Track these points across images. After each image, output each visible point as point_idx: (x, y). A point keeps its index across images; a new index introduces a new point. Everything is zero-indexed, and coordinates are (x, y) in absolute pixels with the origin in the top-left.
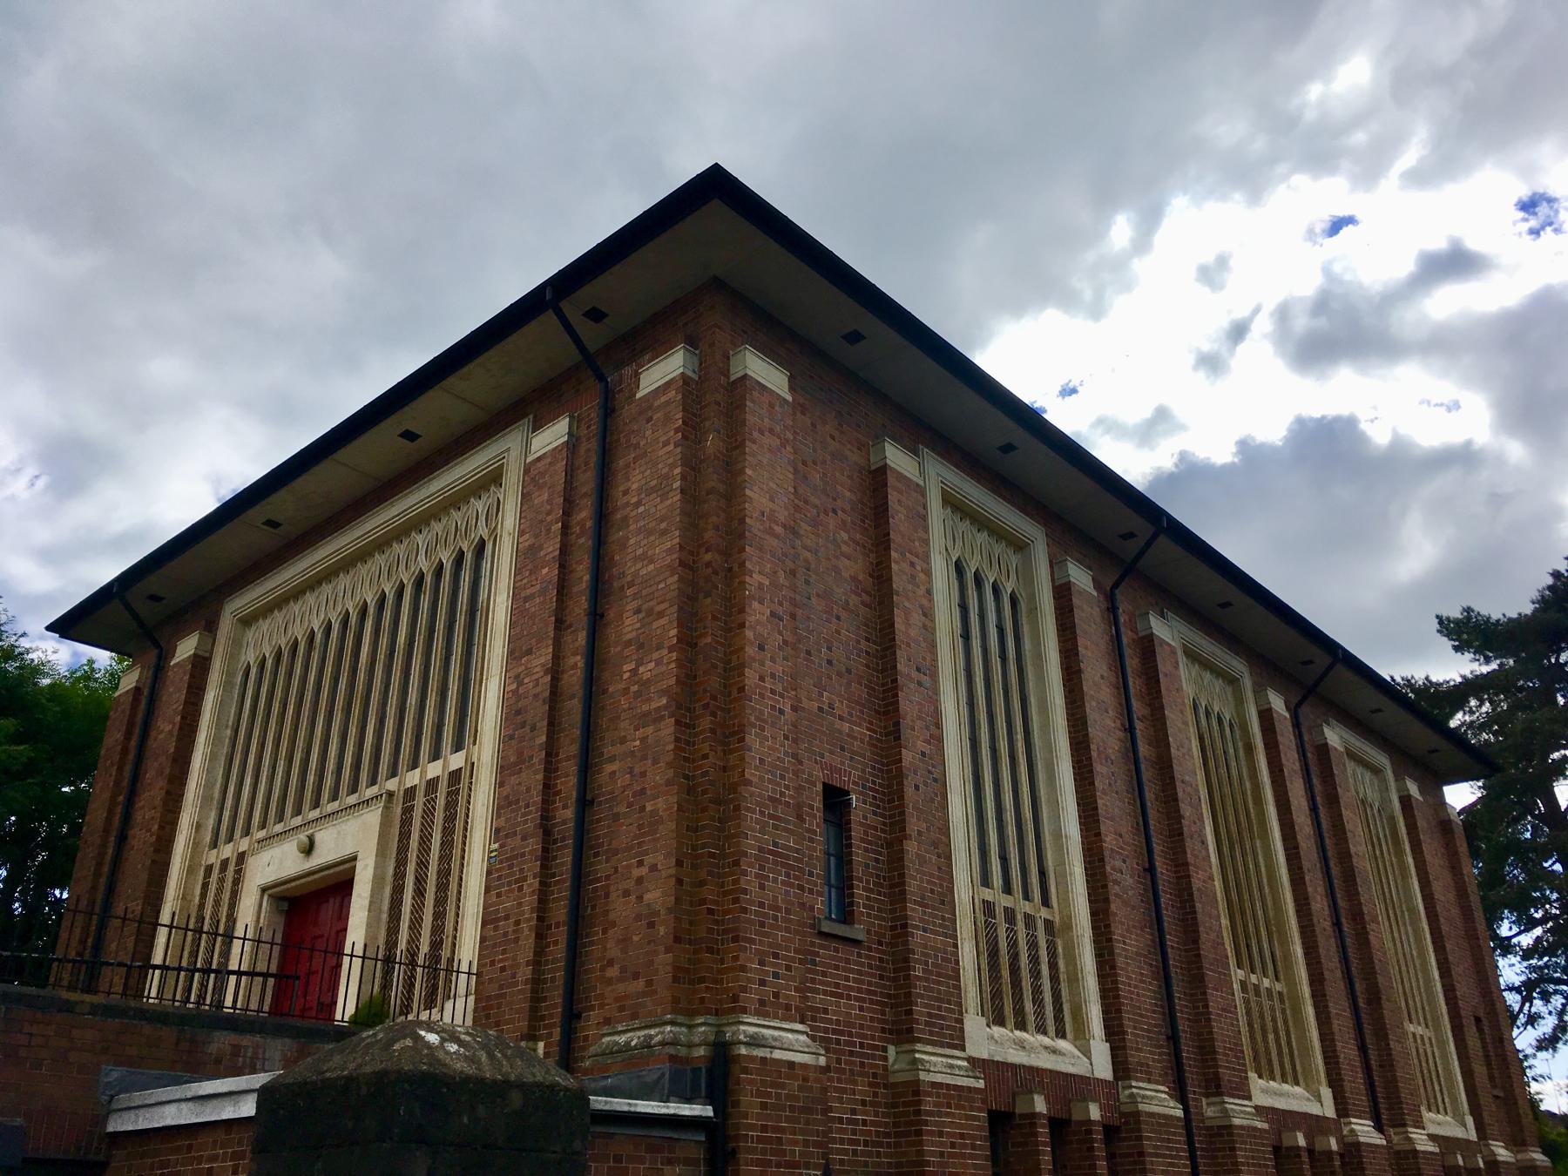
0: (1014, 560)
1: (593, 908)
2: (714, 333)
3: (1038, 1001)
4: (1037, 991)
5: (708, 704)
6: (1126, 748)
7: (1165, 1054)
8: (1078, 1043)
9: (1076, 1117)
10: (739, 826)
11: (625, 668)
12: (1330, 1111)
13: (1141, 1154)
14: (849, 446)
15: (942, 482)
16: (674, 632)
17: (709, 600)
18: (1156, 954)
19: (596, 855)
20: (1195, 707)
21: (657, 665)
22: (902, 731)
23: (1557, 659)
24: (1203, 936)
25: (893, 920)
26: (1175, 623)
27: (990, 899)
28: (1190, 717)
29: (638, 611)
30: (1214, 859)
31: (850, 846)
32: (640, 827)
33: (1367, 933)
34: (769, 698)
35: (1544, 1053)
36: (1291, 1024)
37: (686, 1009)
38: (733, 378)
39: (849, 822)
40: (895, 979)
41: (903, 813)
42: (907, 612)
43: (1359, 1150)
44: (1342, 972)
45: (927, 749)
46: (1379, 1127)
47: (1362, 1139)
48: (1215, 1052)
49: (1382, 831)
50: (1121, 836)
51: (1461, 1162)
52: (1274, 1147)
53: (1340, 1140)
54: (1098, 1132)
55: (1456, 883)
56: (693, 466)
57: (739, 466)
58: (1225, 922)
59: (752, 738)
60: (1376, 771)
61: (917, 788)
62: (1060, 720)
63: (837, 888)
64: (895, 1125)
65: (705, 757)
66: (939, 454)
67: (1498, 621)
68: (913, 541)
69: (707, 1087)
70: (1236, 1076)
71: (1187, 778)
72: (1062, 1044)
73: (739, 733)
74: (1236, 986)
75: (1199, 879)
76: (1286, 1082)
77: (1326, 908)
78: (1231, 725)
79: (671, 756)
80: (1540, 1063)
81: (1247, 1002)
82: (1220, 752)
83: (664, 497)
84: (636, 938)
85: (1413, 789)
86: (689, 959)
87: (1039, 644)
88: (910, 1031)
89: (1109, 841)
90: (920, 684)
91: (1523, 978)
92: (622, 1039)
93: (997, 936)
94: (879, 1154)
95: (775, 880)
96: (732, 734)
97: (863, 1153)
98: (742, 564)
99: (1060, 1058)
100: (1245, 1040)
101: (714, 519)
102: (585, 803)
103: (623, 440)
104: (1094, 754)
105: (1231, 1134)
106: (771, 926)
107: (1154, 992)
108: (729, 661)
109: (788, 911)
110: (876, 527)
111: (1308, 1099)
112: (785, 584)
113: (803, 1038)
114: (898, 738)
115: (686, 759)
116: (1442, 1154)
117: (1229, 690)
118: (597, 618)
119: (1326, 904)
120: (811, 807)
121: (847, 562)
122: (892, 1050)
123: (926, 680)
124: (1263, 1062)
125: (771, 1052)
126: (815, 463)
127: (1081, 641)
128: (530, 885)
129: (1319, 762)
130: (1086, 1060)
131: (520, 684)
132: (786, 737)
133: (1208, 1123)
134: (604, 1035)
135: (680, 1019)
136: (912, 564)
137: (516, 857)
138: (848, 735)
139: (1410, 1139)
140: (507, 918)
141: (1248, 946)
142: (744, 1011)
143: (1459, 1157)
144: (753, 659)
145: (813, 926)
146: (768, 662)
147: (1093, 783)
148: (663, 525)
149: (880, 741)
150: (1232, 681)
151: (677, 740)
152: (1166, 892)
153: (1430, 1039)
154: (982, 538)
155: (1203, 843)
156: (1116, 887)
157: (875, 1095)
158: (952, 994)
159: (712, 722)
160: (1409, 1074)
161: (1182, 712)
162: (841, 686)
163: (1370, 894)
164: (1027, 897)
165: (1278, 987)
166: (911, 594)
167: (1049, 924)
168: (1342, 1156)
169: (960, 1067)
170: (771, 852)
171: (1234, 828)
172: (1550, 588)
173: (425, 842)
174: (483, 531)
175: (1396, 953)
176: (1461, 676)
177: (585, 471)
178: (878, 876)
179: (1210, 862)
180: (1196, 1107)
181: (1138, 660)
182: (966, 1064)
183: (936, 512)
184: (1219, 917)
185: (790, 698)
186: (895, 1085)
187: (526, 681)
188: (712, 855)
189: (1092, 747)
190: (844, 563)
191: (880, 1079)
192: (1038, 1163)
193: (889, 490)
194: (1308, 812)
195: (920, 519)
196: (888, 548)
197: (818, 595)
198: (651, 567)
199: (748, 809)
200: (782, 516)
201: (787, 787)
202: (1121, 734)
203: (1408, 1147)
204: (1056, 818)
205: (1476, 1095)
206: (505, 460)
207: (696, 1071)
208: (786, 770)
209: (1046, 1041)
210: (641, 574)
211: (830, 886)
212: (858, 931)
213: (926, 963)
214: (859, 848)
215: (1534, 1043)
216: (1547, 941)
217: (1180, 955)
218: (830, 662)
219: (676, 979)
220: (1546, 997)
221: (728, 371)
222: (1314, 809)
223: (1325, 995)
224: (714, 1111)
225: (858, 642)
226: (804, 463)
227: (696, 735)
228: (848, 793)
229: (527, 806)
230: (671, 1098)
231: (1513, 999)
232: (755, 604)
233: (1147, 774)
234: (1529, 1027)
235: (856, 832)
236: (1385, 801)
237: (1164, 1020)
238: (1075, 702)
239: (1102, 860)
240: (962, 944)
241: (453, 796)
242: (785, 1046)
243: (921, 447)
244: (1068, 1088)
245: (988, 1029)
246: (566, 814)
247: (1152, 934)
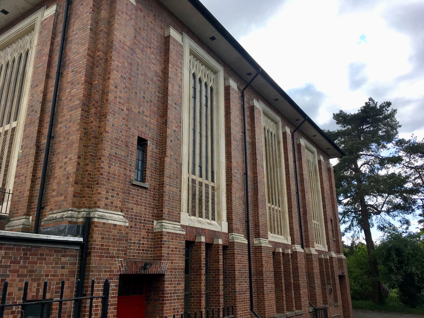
0: (213, 76)
1: (51, 172)
4: (207, 206)
6: (242, 138)
8: (219, 222)
9: (215, 243)
10: (102, 146)
11: (67, 91)
12: (290, 243)
13: (234, 254)
14: (157, 27)
16: (84, 78)
17: (97, 69)
18: (245, 198)
19: (53, 155)
20: (265, 129)
22: (168, 123)
24: (259, 193)
25: (159, 182)
26: (261, 103)
27: (195, 178)
29: (73, 71)
30: (265, 172)
31: (146, 158)
32: (67, 145)
33: (305, 196)
34: (118, 105)
36: (282, 219)
37: (77, 206)
39: (147, 150)
41: (166, 149)
42: (173, 85)
43: (296, 253)
46: (303, 247)
47: (297, 250)
48: (259, 226)
49: (312, 168)
50: (238, 163)
51: (323, 257)
52: (273, 252)
53: (292, 250)
54: (221, 247)
55: (330, 184)
56: (96, 22)
57: (113, 23)
58: (266, 190)
59: (110, 117)
60: (313, 153)
61: (171, 141)
62: (222, 127)
63: (141, 171)
65: (92, 122)
66: (190, 37)
67: (349, 115)
68: (177, 62)
69: (82, 231)
70: (264, 232)
71: (260, 148)
72: (213, 222)
74: (267, 208)
75: (260, 177)
77: (295, 188)
78: (274, 136)
79: (79, 121)
81: (270, 212)
82: (270, 143)
83: (85, 31)
84: (63, 182)
85: (322, 158)
88: (162, 216)
89: (234, 164)
90: (175, 108)
92: (54, 216)
96: (103, 115)
97: (142, 253)
98: (111, 57)
99: (212, 226)
101: (102, 40)
102: (51, 137)
103: (74, 13)
104: (232, 138)
105: (261, 248)
106: (112, 180)
107: (243, 208)
108: (104, 91)
109: (119, 176)
110: (165, 56)
111: (284, 239)
112: (128, 67)
113: (122, 217)
114: (166, 125)
116: (318, 255)
117: (275, 125)
118: (60, 74)
121: (154, 66)
122: (155, 222)
123: (178, 108)
124: (273, 228)
125: (107, 221)
126: (144, 30)
127: (231, 104)
128: (30, 165)
129: (297, 149)
130: (220, 226)
131: (33, 97)
132: (123, 119)
134: (49, 214)
135: (75, 209)
136: (176, 70)
137: (27, 155)
139: (310, 251)
140: (23, 175)
142: (99, 207)
143: (323, 256)
145: (130, 182)
146: (118, 93)
147: (231, 147)
148: (83, 41)
150: (276, 123)
151: (82, 115)
154: (203, 67)
155: (262, 167)
157: (148, 235)
158: (177, 206)
159: (95, 110)
162: (148, 106)
163: (307, 185)
164: (201, 176)
165: (279, 209)
166: (175, 79)
167: (213, 188)
168: (292, 255)
169: (177, 228)
170: (114, 156)
171: (272, 165)
173: (3, 151)
174: (28, 47)
175: (312, 202)
176: (337, 130)
177: (60, 24)
178: (155, 168)
182: (180, 227)
183: (187, 57)
184: (264, 188)
185: (126, 106)
186: (155, 233)
187: (35, 96)
188: (91, 155)
189: (232, 136)
190: (152, 65)
191: (150, 231)
192: (201, 256)
193: (170, 44)
195: (181, 56)
196: (168, 63)
197: (141, 74)
198: (78, 56)
200: (128, 43)
202: (241, 134)
203: (310, 253)
206: (36, 22)
208: (123, 130)
209: (208, 221)
211: (138, 170)
212: (146, 185)
213: (169, 196)
214: (150, 158)
216: (351, 202)
218: (144, 97)
219: (74, 196)
222: (295, 161)
223: (292, 212)
224: (83, 240)
225: (155, 92)
226: (140, 29)
227: (89, 115)
229: (32, 138)
230: (68, 235)
231: (340, 217)
232: (115, 72)
233: (248, 146)
234: (343, 224)
235: (149, 153)
236: (314, 161)
238: (228, 122)
239: (231, 169)
240: (183, 191)
241: (12, 135)
242: (114, 219)
243: (184, 33)
244: (214, 234)
245: (189, 217)
246: (44, 141)
247: (245, 192)
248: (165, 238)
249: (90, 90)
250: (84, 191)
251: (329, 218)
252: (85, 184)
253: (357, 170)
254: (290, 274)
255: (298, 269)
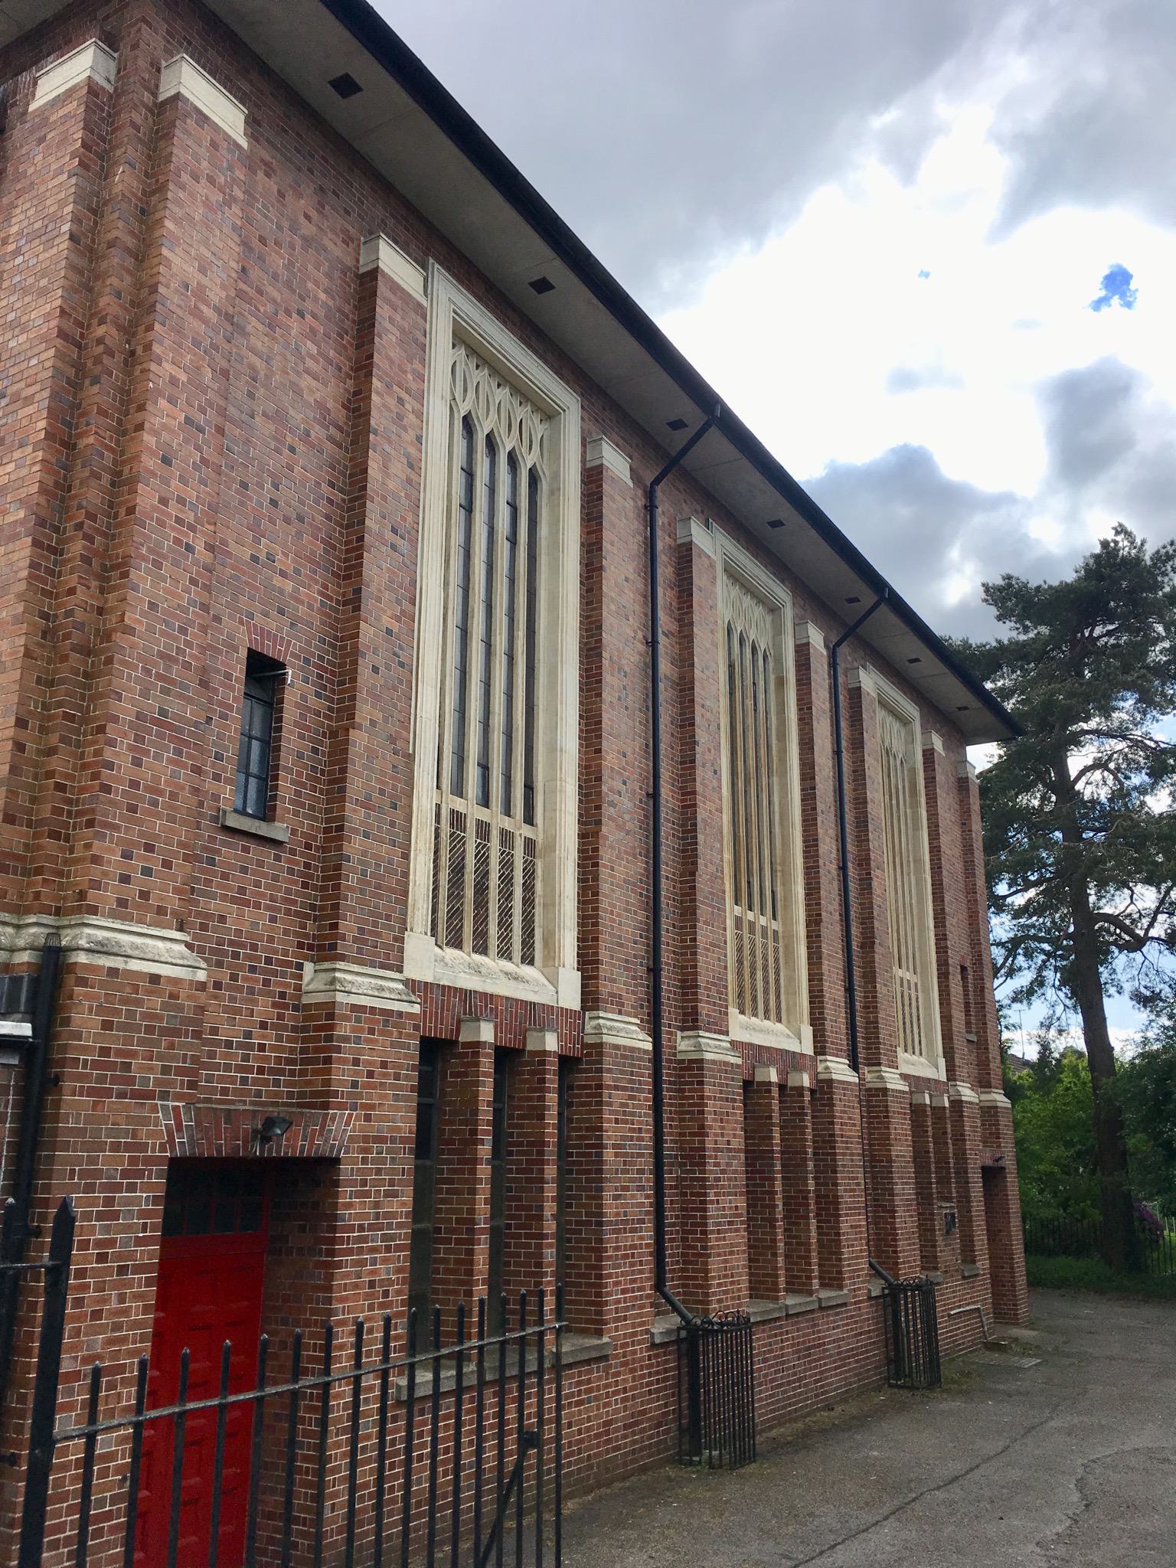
0: (540, 430)
2: (140, 29)
3: (505, 923)
4: (505, 914)
5: (82, 523)
6: (645, 664)
7: (642, 985)
8: (545, 970)
9: (530, 1046)
12: (808, 1049)
14: (330, 234)
15: (456, 313)
16: (42, 424)
17: (96, 389)
21: (17, 467)
23: (1091, 632)
25: (328, 821)
26: (719, 536)
27: (462, 810)
28: (721, 639)
31: (279, 729)
34: (173, 528)
35: (1019, 1004)
36: (782, 961)
38: (161, 98)
40: (324, 888)
41: (353, 698)
44: (840, 915)
45: (395, 627)
46: (854, 1066)
47: (834, 1077)
48: (696, 986)
49: (900, 781)
51: (928, 1102)
52: (745, 1082)
53: (815, 1076)
57: (157, 216)
58: (728, 856)
59: (141, 576)
60: (905, 722)
61: (375, 670)
64: (303, 1051)
65: (72, 591)
68: (405, 372)
70: (715, 1011)
71: (708, 703)
72: (527, 971)
73: (122, 568)
74: (730, 923)
75: (705, 810)
76: (769, 1019)
77: (834, 851)
78: (765, 658)
80: (1014, 1014)
82: (749, 682)
83: (49, 244)
85: (937, 743)
86: (26, 845)
87: (558, 531)
88: (334, 947)
90: (394, 547)
91: (1011, 935)
93: (464, 851)
94: (277, 1083)
95: (157, 756)
96: (113, 568)
97: (255, 1082)
98: (148, 347)
99: (521, 986)
100: (731, 977)
104: (605, 663)
105: (702, 1069)
106: (146, 812)
109: (173, 796)
112: (211, 385)
113: (182, 948)
114: (358, 609)
115: (44, 592)
117: (769, 618)
119: (834, 847)
120: (228, 676)
122: (309, 967)
123: (403, 545)
125: (126, 962)
130: (551, 987)
132: (193, 582)
133: (679, 1057)
138: (292, 597)
139: (882, 1078)
141: (749, 883)
142: (93, 911)
143: (927, 1096)
144: (154, 474)
145: (215, 819)
146: (175, 483)
147: (600, 695)
148: (44, 282)
149: (337, 611)
150: (774, 610)
151: (33, 565)
152: (668, 821)
153: (916, 984)
154: (502, 394)
155: (715, 772)
156: (611, 809)
157: (280, 1017)
160: (890, 1016)
161: (712, 632)
163: (879, 842)
166: (394, 437)
167: (530, 845)
168: (812, 1091)
169: (391, 990)
171: (752, 763)
172: (1097, 557)
179: (720, 792)
180: (669, 1040)
181: (672, 569)
182: (401, 986)
183: (442, 353)
186: (308, 1007)
190: (306, 382)
193: (379, 302)
194: (830, 753)
195: (418, 347)
196: (370, 374)
197: (264, 414)
198: (23, 338)
199: (124, 663)
200: (216, 295)
201: (188, 644)
202: (642, 648)
203: (879, 1086)
204: (553, 728)
205: (951, 1039)
207: (16, 981)
208: (191, 623)
210: (10, 346)
211: (248, 775)
212: (278, 830)
213: (364, 873)
214: (291, 732)
215: (1012, 995)
217: (674, 887)
218: (274, 503)
220: (1029, 955)
221: (157, 86)
222: (837, 753)
226: (262, 240)
227: (64, 563)
228: (283, 666)
231: (998, 954)
232: (163, 403)
233: (665, 693)
235: (290, 713)
236: (909, 754)
237: (647, 952)
238: (591, 603)
239: (599, 779)
240: (416, 855)
242: (150, 956)
243: (431, 260)
244: (533, 1015)
245: (437, 949)
247: (647, 863)
248: (344, 1029)
249: (68, 468)
250: (39, 847)
251: (954, 961)
252: (42, 822)
253: (1065, 787)
254: (805, 1160)
255: (835, 1142)
